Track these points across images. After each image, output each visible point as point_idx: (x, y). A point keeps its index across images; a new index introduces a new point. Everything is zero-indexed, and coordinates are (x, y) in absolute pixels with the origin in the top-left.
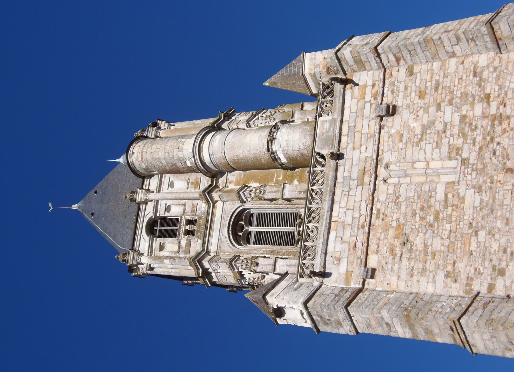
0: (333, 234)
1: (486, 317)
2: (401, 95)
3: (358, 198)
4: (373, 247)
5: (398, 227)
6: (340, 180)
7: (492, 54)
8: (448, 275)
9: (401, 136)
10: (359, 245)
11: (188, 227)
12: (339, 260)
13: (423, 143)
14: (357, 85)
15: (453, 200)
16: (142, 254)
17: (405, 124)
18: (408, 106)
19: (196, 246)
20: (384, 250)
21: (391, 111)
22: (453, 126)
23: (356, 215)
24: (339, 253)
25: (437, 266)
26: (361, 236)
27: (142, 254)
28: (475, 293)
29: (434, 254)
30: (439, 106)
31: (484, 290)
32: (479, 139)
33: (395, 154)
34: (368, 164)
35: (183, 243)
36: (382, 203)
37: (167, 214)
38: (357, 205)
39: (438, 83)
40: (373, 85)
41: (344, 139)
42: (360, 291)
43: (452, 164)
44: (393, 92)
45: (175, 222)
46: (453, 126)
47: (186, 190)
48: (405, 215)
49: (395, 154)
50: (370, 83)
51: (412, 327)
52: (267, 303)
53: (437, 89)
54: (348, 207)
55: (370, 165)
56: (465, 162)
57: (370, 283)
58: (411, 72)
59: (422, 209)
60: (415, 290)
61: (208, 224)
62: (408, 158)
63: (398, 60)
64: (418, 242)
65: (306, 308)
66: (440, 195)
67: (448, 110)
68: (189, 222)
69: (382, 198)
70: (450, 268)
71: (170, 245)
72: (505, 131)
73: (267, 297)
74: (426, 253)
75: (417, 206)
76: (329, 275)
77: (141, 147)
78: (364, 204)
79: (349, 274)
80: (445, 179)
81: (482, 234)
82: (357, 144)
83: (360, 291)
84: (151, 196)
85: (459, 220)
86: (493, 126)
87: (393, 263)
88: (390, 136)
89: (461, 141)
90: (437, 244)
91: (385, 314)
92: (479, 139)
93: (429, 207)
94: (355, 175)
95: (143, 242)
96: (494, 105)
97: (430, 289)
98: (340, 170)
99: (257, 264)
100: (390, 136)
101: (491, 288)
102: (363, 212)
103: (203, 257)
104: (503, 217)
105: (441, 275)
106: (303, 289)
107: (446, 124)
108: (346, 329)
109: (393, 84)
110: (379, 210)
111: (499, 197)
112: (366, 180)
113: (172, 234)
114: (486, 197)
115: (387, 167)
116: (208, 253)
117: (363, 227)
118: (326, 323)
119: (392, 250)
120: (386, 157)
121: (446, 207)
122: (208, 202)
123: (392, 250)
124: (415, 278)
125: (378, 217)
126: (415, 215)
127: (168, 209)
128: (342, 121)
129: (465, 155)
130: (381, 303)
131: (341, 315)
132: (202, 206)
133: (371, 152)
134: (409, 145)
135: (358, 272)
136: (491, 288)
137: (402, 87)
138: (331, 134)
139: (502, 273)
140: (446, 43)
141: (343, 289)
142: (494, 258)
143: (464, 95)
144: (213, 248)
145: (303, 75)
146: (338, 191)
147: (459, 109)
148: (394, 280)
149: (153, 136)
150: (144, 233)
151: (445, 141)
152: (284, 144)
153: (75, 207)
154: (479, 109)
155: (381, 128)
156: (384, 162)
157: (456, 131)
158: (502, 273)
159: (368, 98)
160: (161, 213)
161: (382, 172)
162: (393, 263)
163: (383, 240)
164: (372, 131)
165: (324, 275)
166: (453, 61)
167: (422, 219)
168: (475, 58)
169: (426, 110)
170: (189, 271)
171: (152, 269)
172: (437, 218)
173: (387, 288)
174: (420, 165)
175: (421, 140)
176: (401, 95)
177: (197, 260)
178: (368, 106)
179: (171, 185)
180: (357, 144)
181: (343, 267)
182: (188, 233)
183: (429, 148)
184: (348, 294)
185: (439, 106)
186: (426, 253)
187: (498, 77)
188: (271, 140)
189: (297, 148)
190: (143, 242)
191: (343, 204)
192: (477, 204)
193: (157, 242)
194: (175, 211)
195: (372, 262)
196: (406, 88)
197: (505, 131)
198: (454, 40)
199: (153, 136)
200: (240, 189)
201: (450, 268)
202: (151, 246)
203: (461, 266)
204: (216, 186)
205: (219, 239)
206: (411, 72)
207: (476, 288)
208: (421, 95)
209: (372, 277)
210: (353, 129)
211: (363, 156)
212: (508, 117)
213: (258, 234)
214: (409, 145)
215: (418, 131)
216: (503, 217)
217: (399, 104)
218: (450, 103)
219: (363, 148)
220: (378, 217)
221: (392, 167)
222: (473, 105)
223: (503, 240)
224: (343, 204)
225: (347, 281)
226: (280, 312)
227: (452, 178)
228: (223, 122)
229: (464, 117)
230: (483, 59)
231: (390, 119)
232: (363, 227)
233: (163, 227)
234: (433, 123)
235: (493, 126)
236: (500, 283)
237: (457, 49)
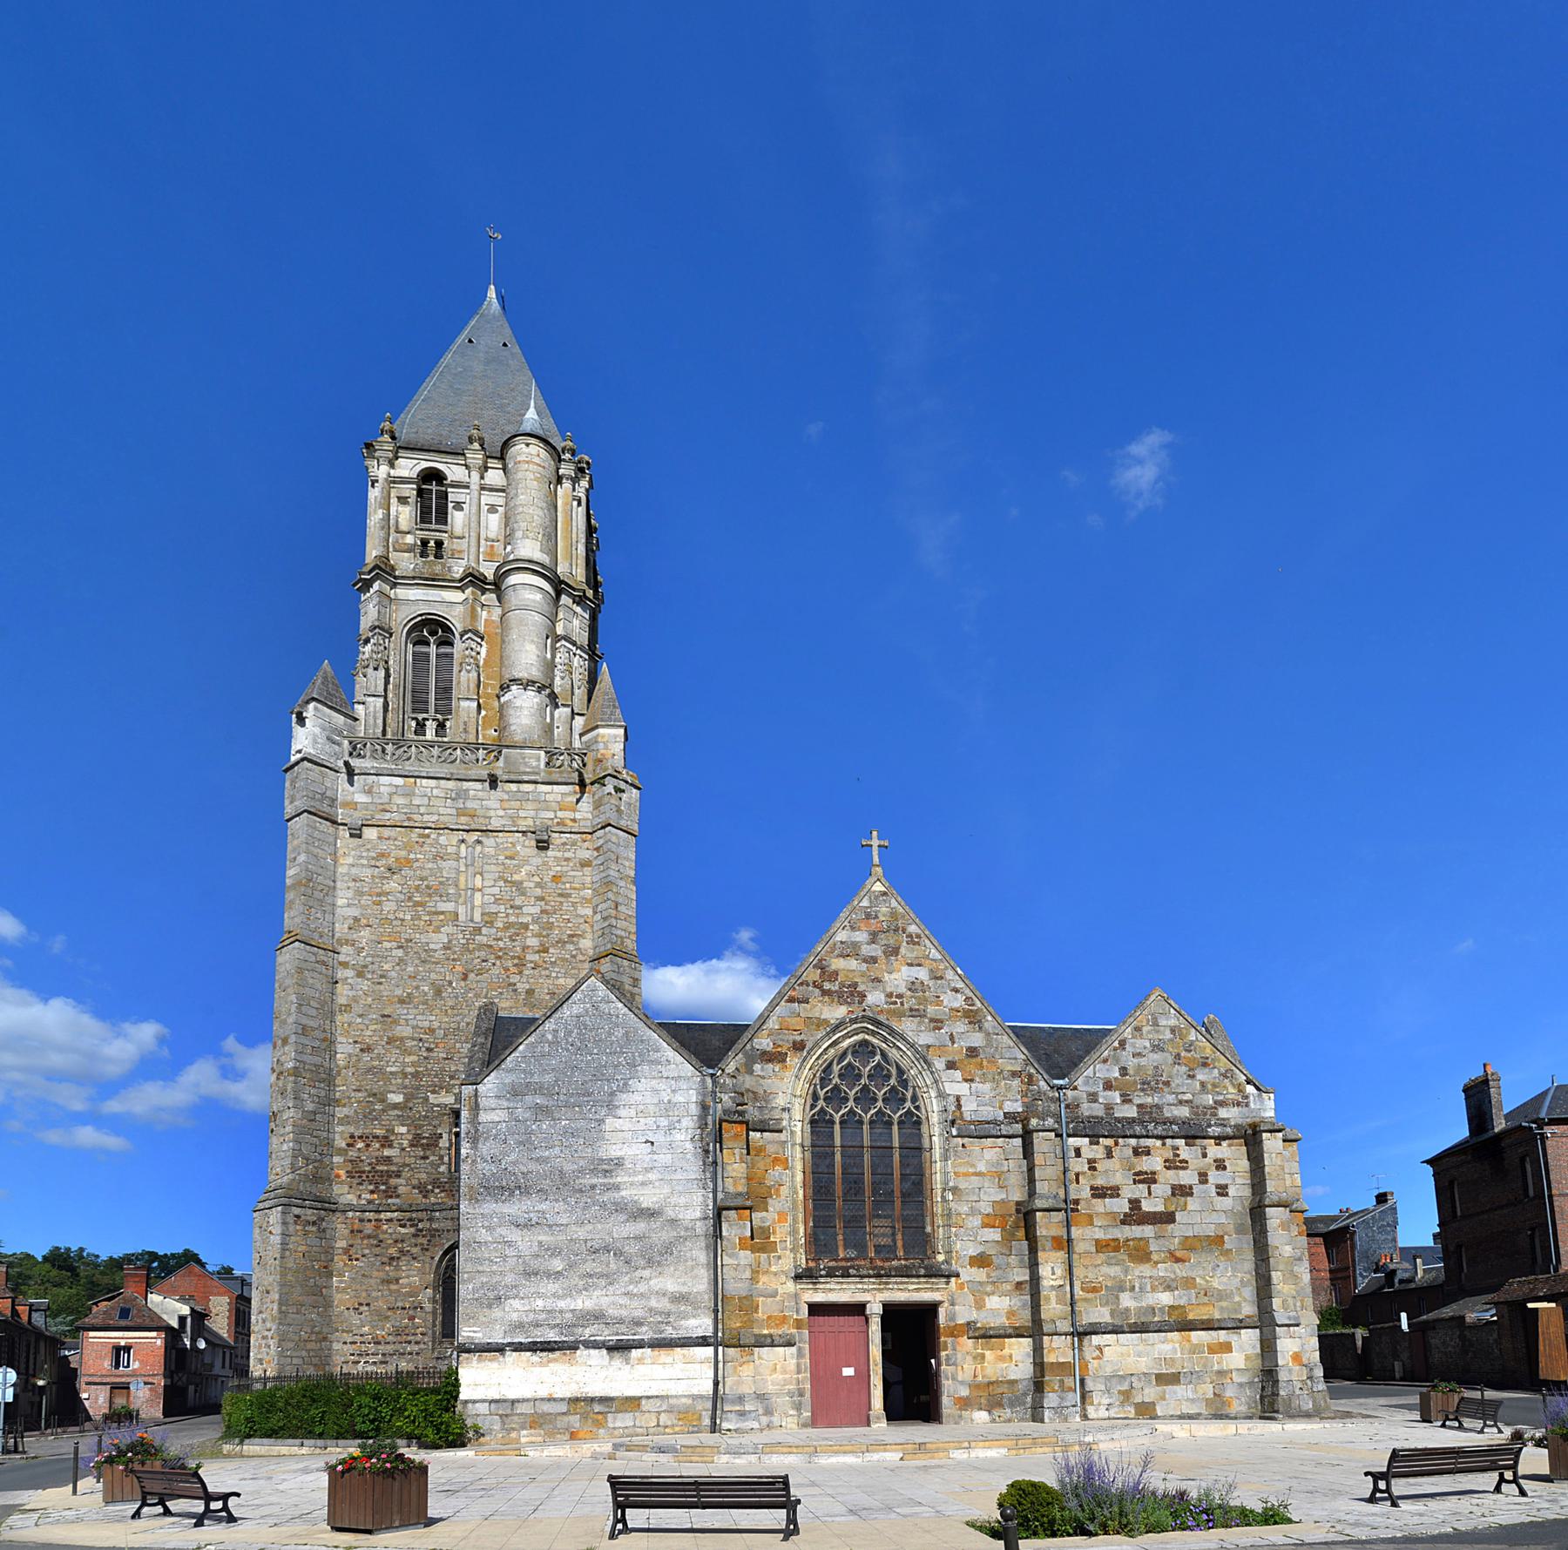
0: (399, 781)
1: (304, 965)
2: (559, 854)
3: (442, 810)
4: (387, 832)
5: (408, 861)
6: (466, 785)
7: (591, 952)
8: (356, 919)
9: (511, 858)
10: (388, 816)
11: (432, 543)
12: (369, 792)
13: (501, 883)
14: (578, 801)
15: (437, 920)
16: (392, 466)
17: (526, 862)
18: (545, 863)
19: (405, 563)
20: (383, 847)
21: (543, 845)
22: (517, 916)
23: (422, 810)
24: (375, 791)
25: (364, 907)
26: (396, 817)
27: (392, 466)
28: (339, 949)
29: (379, 903)
30: (542, 899)
31: (342, 958)
32: (501, 944)
33: (492, 851)
34: (481, 820)
35: (409, 539)
36: (436, 841)
37: (450, 505)
38: (434, 810)
39: (569, 895)
40: (574, 820)
41: (513, 787)
42: (334, 822)
43: (477, 917)
44: (564, 844)
45: (443, 517)
46: (517, 916)
47: (483, 536)
48: (422, 868)
49: (492, 851)
50: (578, 815)
51: (294, 886)
52: (308, 702)
53: (561, 895)
54: (432, 796)
55: (479, 823)
56: (478, 931)
57: (344, 833)
58: (585, 864)
59: (428, 887)
60: (339, 884)
61: (431, 581)
62: (487, 867)
63: (597, 849)
64: (392, 885)
65: (303, 759)
66: (442, 906)
67: (536, 910)
68: (439, 544)
69: (442, 840)
70: (364, 921)
71: (405, 515)
72: (507, 969)
73: (312, 706)
74: (379, 895)
75: (433, 882)
76: (351, 783)
77: (537, 460)
78: (435, 818)
79: (354, 805)
80: (461, 910)
81: (400, 953)
82: (506, 805)
83: (334, 822)
84: (475, 476)
85: (416, 928)
86: (513, 958)
87: (367, 858)
88: (513, 844)
89: (500, 925)
90: (389, 907)
91: (302, 858)
92: (501, 944)
93: (430, 895)
94: (469, 804)
95: (409, 467)
96: (536, 957)
97: (340, 902)
98: (478, 785)
99: (376, 669)
100: (513, 844)
101: (345, 965)
102: (426, 818)
103: (385, 581)
104: (417, 973)
105: (355, 912)
106: (329, 748)
107: (520, 908)
108: (289, 810)
109: (574, 844)
110: (428, 836)
111: (439, 968)
112: (463, 819)
113: (424, 517)
114: (439, 955)
115: (479, 842)
116: (393, 586)
117: (409, 819)
118: (293, 782)
119: (383, 855)
120: (489, 841)
121: (429, 913)
122: (461, 580)
123: (382, 855)
124: (352, 884)
125: (421, 836)
126: (422, 879)
127: (459, 506)
128: (535, 782)
129: (484, 931)
130: (316, 851)
131: (300, 804)
132: (458, 571)
133: (496, 824)
134: (500, 868)
135: (356, 818)
136: (345, 965)
137: (567, 855)
138: (522, 769)
139: (360, 975)
140: (604, 906)
141: (334, 800)
142: (375, 967)
143: (550, 926)
144: (401, 592)
145: (597, 727)
146: (451, 784)
147: (535, 921)
148: (349, 858)
149: (561, 472)
150: (425, 465)
151: (502, 908)
152: (518, 703)
153: (492, 293)
154: (533, 942)
155: (523, 832)
156: (483, 839)
157: (512, 919)
158: (360, 975)
159: (560, 814)
160: (454, 495)
161: (474, 836)
162: (367, 858)
163: (395, 845)
164: (521, 822)
165: (351, 773)
166: (589, 912)
167: (417, 888)
168: (589, 936)
169: (538, 885)
170: (372, 553)
171: (373, 483)
172: (417, 904)
173: (341, 852)
174: (478, 882)
175: (506, 881)
176: (559, 854)
177: (384, 570)
178: (551, 815)
179: (493, 509)
180: (506, 805)
181: (361, 798)
182: (425, 543)
183: (496, 890)
184: (327, 809)
185: (542, 899)
186: (379, 895)
187: (564, 960)
188: (527, 684)
189: (512, 721)
190: (409, 467)
191: (435, 792)
192: (432, 946)
193: (410, 491)
194: (457, 519)
195: (370, 834)
196: (567, 860)
197: (507, 969)
198: (605, 914)
199: (561, 472)
200: (476, 633)
201: (364, 921)
202: (404, 481)
203: (365, 933)
204: (484, 592)
205: (416, 600)
206: (585, 864)
207: (345, 949)
208: (556, 878)
209: (352, 835)
210: (524, 798)
211: (492, 813)
212: (520, 973)
213: (427, 655)
214: (500, 868)
215: (516, 877)
216: (417, 973)
217: (549, 853)
218: (542, 912)
219: (501, 813)
220: (421, 836)
221: (479, 848)
222: (539, 935)
223: (393, 974)
224: (435, 792)
225: (346, 805)
226: (301, 720)
227: (462, 918)
228: (570, 595)
229: (526, 926)
230: (586, 944)
231: (534, 843)
232: (409, 819)
233: (432, 495)
234: (523, 894)
235: (513, 958)
236: (349, 973)
237: (598, 917)
